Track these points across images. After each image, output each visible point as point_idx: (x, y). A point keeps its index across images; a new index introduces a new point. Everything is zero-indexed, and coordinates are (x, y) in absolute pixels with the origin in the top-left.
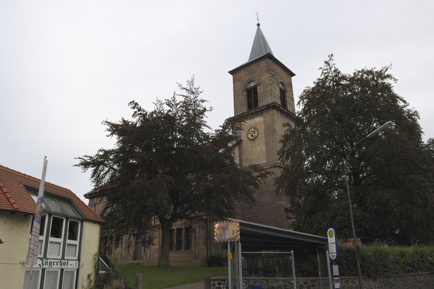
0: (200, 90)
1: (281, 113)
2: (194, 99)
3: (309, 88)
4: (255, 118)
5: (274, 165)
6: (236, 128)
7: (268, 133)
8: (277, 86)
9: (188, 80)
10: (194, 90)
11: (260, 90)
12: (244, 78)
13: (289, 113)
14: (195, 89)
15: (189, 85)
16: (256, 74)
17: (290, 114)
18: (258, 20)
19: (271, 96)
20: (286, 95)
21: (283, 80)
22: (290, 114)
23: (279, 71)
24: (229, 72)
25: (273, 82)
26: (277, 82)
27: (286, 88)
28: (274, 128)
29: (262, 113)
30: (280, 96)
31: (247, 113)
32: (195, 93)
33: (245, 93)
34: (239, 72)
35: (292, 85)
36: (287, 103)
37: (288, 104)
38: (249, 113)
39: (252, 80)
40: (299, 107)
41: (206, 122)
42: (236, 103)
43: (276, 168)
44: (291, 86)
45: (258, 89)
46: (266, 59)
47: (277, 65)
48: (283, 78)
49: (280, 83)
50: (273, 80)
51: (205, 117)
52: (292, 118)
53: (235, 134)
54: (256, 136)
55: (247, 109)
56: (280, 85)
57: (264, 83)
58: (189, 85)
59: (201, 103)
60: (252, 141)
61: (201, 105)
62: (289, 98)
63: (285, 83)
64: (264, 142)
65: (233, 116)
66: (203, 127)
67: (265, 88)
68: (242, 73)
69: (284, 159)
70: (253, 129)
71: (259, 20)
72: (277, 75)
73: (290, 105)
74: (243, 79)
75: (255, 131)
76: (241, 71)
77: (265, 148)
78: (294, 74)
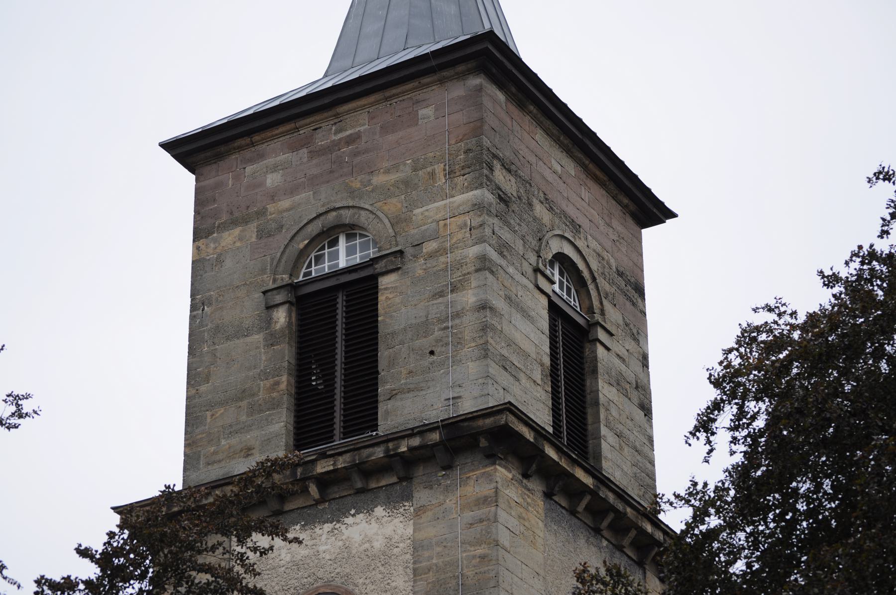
1: (548, 495)
3: (780, 315)
4: (349, 520)
11: (398, 300)
12: (285, 203)
13: (611, 497)
16: (379, 179)
17: (616, 511)
19: (485, 353)
21: (580, 244)
22: (620, 506)
24: (168, 146)
25: (503, 248)
26: (533, 259)
27: (596, 303)
29: (401, 480)
30: (547, 361)
33: (281, 316)
34: (248, 154)
36: (597, 421)
37: (604, 431)
38: (299, 470)
39: (344, 225)
40: (711, 451)
42: (203, 388)
45: (382, 298)
47: (540, 124)
50: (506, 235)
52: (626, 542)
56: (557, 277)
63: (594, 265)
67: (441, 294)
68: (270, 161)
72: (535, 202)
73: (619, 435)
74: (271, 208)
78: (660, 205)
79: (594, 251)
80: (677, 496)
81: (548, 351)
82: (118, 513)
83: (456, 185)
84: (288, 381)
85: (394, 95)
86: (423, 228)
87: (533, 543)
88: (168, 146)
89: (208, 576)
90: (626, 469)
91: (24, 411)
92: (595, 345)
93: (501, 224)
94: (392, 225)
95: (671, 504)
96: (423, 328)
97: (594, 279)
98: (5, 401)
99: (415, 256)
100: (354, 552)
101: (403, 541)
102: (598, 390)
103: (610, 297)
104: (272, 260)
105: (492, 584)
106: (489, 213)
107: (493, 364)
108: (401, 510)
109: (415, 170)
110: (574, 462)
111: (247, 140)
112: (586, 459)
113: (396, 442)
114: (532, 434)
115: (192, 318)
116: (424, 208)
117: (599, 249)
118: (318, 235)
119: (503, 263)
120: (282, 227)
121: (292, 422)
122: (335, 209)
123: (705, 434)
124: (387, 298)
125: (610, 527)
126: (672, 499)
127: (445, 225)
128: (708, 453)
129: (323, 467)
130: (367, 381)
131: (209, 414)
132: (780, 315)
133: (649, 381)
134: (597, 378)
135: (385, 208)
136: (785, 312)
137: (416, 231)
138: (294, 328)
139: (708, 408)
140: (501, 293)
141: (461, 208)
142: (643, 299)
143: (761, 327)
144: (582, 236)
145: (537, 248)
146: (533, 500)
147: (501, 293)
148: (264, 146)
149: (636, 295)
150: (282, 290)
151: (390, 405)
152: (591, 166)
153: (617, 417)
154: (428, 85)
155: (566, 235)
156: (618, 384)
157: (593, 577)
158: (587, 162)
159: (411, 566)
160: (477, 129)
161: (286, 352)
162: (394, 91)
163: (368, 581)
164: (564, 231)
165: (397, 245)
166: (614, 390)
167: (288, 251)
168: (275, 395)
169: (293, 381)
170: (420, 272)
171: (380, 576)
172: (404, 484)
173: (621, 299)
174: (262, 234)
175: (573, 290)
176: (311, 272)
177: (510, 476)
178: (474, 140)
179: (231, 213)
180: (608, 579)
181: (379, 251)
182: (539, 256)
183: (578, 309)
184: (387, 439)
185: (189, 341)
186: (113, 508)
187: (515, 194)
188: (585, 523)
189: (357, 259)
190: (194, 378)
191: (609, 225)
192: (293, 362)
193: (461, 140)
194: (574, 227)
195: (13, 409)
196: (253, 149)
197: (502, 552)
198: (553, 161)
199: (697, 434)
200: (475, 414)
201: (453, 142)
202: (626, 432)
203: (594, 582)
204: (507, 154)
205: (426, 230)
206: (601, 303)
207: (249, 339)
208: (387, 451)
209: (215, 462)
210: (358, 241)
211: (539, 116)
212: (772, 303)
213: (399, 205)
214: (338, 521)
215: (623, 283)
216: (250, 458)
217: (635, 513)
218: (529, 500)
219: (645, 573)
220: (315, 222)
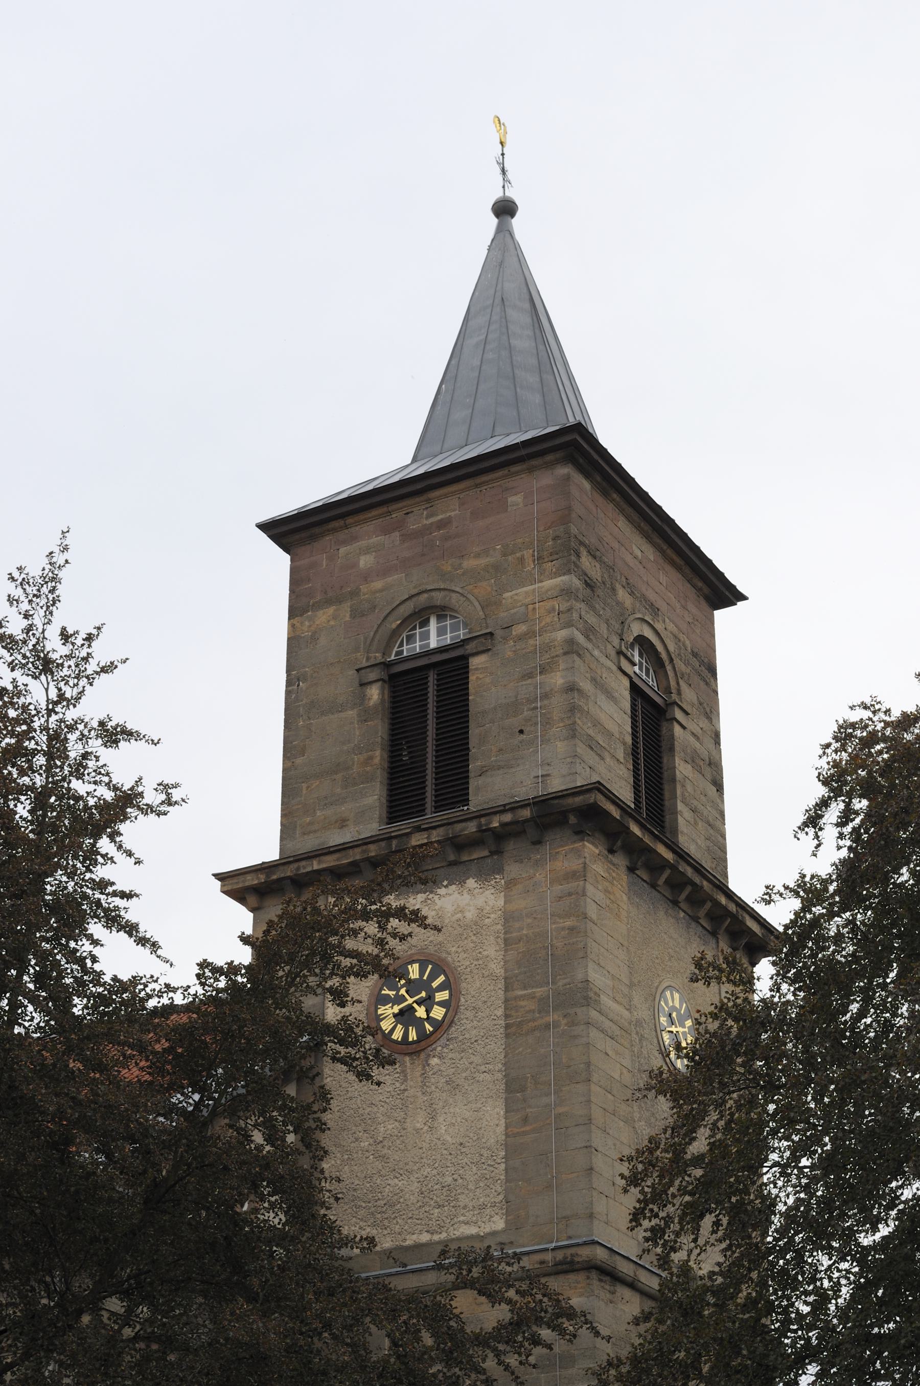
0: (101, 653)
1: (631, 869)
2: (49, 716)
3: (874, 712)
4: (442, 891)
5: (560, 1255)
6: (347, 962)
7: (533, 1011)
8: (614, 668)
9: (20, 569)
10: (55, 647)
11: (488, 680)
12: (378, 584)
13: (689, 872)
14: (65, 636)
15: (25, 606)
16: (469, 563)
17: (693, 884)
18: (503, 171)
19: (573, 733)
20: (672, 737)
21: (659, 626)
22: (697, 879)
23: (629, 559)
24: (265, 527)
25: (589, 632)
26: (616, 641)
27: (673, 683)
28: (580, 976)
29: (492, 853)
30: (629, 740)
31: (383, 844)
32: (66, 672)
33: (375, 694)
34: (342, 535)
35: (712, 670)
36: (675, 797)
37: (680, 806)
38: (394, 843)
39: (436, 607)
40: (818, 846)
41: (125, 895)
42: (299, 761)
43: (581, 1277)
44: (706, 673)
45: (472, 678)
46: (550, 465)
47: (622, 511)
48: (655, 611)
49: (632, 646)
50: (592, 619)
51: (119, 856)
52: (702, 913)
53: (342, 1005)
54: (438, 1025)
55: (385, 815)
56: (637, 659)
57: (520, 638)
58: (25, 606)
59: (95, 745)
60: (407, 1059)
61: (100, 764)
62: (693, 759)
63: (672, 647)
64: (499, 1076)
65: (272, 853)
66: (96, 928)
67: (530, 675)
68: (363, 543)
69: (668, 1219)
70: (416, 966)
71: (510, 175)
72: (618, 586)
73: (694, 810)
74: (364, 588)
75: (435, 984)
76: (354, 530)
77: (502, 1122)
78: (732, 588)
79: (671, 633)
80: (786, 888)
81: (630, 730)
82: (219, 879)
83: (544, 570)
84: (381, 756)
85: (484, 482)
86: (512, 611)
87: (618, 916)
88: (265, 527)
89: (355, 961)
90: (700, 843)
91: (174, 799)
92: (672, 723)
93: (587, 609)
94: (483, 608)
95: (781, 895)
96: (513, 707)
97: (671, 660)
98: (156, 789)
99: (505, 638)
100: (447, 921)
101: (494, 912)
102: (675, 767)
103: (686, 677)
104: (366, 639)
105: (581, 954)
106: (577, 598)
107: (580, 744)
108: (492, 882)
109: (505, 555)
110: (657, 838)
111: (341, 522)
112: (662, 832)
113: (487, 818)
114: (619, 811)
115: (288, 693)
116: (514, 592)
117: (675, 630)
118: (411, 616)
119: (589, 646)
120: (375, 607)
121: (385, 795)
122: (426, 591)
123: (813, 830)
124: (477, 678)
125: (688, 899)
126: (782, 890)
127: (534, 609)
128: (816, 848)
129: (417, 840)
130: (459, 757)
131: (304, 785)
132: (874, 712)
133: (720, 758)
134: (674, 756)
135: (476, 591)
136: (879, 710)
137: (505, 614)
138: (387, 705)
139: (817, 804)
140: (587, 675)
141: (549, 593)
142: (716, 679)
143: (856, 723)
144: (660, 618)
145: (620, 631)
146: (618, 874)
147: (587, 675)
148: (357, 528)
149: (709, 675)
150: (376, 669)
151: (481, 781)
152: (669, 552)
153: (692, 793)
154: (517, 473)
155: (646, 618)
156: (693, 761)
157: (710, 964)
158: (665, 548)
159: (502, 936)
160: (565, 516)
161: (380, 729)
162: (484, 478)
163: (460, 950)
164: (644, 614)
165: (487, 627)
166: (689, 766)
167: (380, 631)
168: (368, 769)
169: (386, 756)
170: (509, 654)
171: (472, 945)
172: (495, 857)
173: (696, 679)
174: (357, 613)
175: (651, 671)
176: (402, 651)
177: (597, 851)
178: (562, 528)
179: (326, 593)
180: (724, 966)
181: (470, 633)
182: (622, 639)
183: (656, 689)
184: (479, 816)
185: (285, 715)
186: (214, 875)
187: (600, 579)
188: (664, 896)
189: (448, 639)
190: (291, 750)
191: (684, 607)
192: (386, 737)
193: (549, 528)
194: (653, 610)
195: (163, 797)
196: (346, 531)
197: (590, 925)
198: (634, 547)
199: (806, 829)
200: (565, 793)
201: (541, 529)
202: (700, 807)
203: (711, 969)
204: (592, 540)
205: (515, 613)
206: (678, 683)
207: (342, 715)
208: (480, 825)
209: (310, 832)
210: (448, 622)
211: (622, 503)
212: (868, 701)
213: (489, 589)
214: (431, 892)
215: (697, 664)
216: (345, 829)
217: (711, 886)
218: (614, 874)
219: (718, 942)
220: (408, 603)
